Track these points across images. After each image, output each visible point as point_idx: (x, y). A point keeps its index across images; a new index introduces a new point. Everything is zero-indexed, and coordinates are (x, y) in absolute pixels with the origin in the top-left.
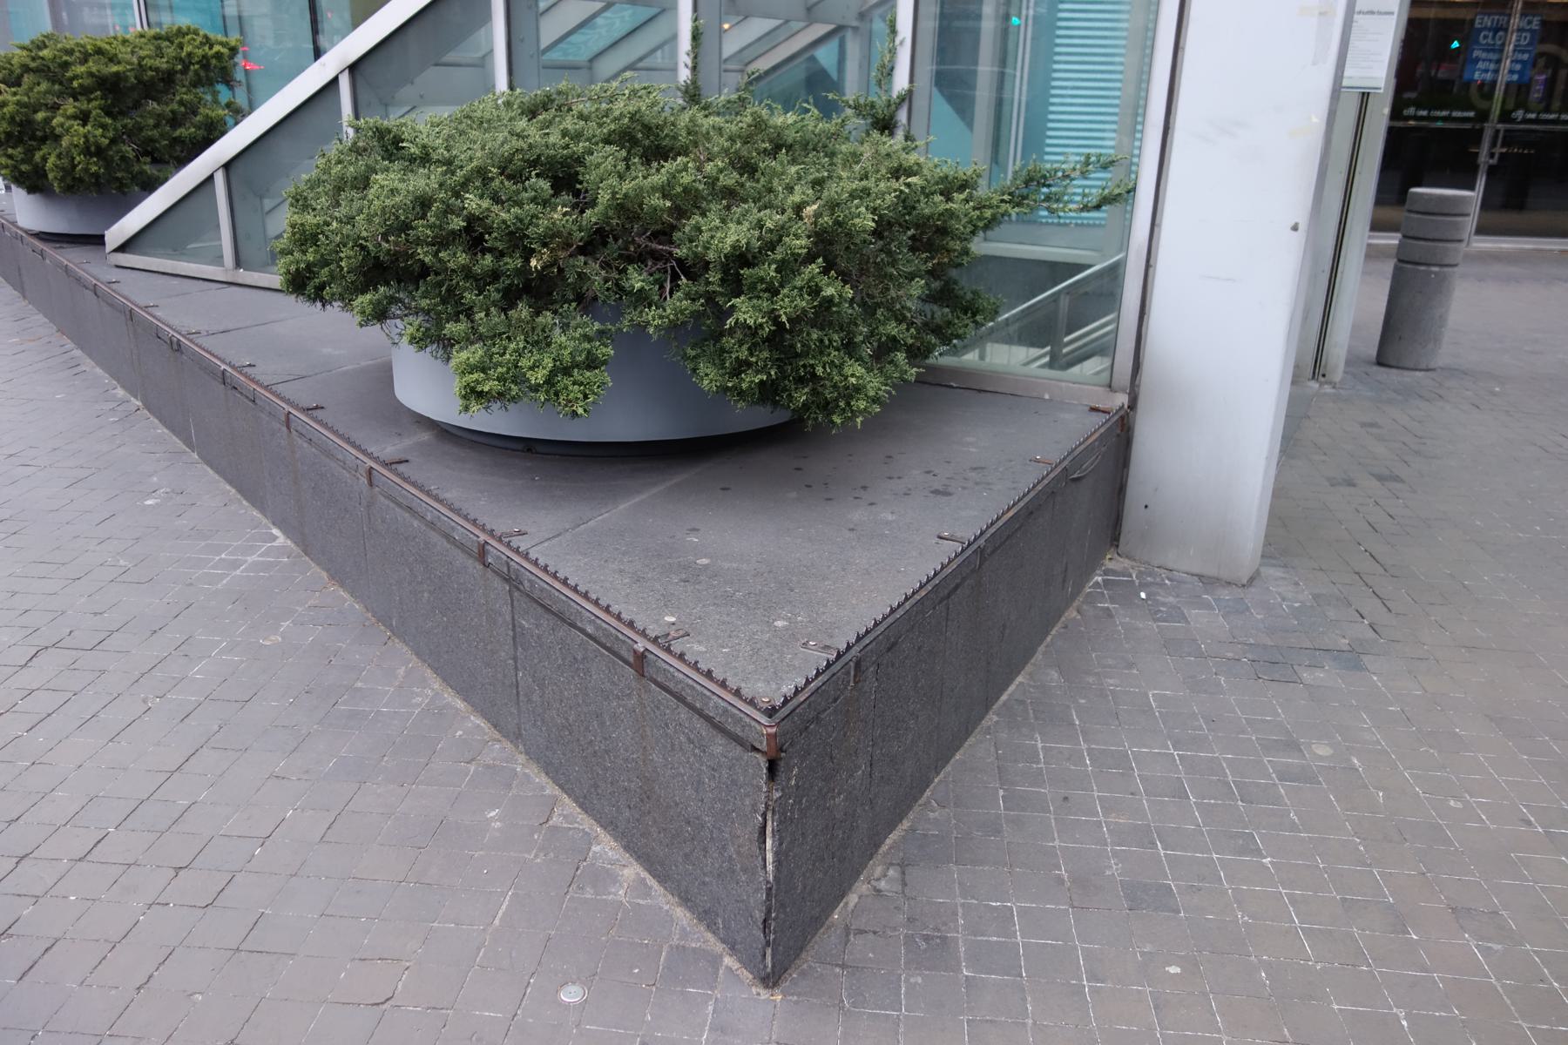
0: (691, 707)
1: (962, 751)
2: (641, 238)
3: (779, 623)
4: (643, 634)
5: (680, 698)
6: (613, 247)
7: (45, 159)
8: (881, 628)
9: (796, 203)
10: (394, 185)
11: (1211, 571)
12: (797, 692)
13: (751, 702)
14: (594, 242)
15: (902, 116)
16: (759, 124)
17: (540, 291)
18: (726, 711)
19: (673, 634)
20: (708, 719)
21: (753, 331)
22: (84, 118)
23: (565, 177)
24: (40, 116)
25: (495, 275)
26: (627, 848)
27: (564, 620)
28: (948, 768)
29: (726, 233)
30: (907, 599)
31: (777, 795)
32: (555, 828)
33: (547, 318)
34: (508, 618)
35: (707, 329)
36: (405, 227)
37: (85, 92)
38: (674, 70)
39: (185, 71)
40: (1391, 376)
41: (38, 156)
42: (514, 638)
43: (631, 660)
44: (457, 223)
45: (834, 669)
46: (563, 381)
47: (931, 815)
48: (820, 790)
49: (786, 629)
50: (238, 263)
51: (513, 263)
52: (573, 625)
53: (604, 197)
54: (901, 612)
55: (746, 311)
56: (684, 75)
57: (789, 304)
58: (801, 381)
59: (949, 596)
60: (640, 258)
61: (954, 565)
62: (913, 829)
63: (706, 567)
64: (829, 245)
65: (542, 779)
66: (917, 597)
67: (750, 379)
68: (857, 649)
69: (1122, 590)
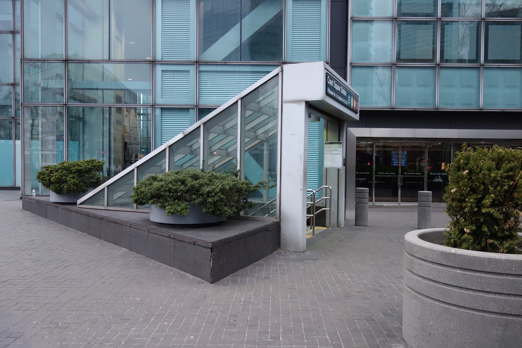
2: (195, 191)
6: (190, 192)
7: (64, 186)
9: (218, 185)
10: (156, 184)
11: (296, 250)
14: (187, 192)
15: (239, 174)
16: (213, 175)
17: (179, 198)
21: (211, 203)
22: (73, 178)
23: (183, 182)
24: (64, 177)
25: (172, 196)
29: (207, 189)
33: (180, 202)
35: (204, 203)
36: (159, 189)
37: (74, 173)
38: (199, 166)
39: (94, 168)
40: (357, 227)
41: (62, 186)
44: (167, 189)
46: (182, 211)
50: (108, 206)
51: (175, 194)
53: (189, 185)
55: (210, 200)
56: (201, 167)
57: (216, 198)
58: (218, 210)
60: (194, 194)
64: (222, 191)
67: (211, 210)
69: (280, 254)
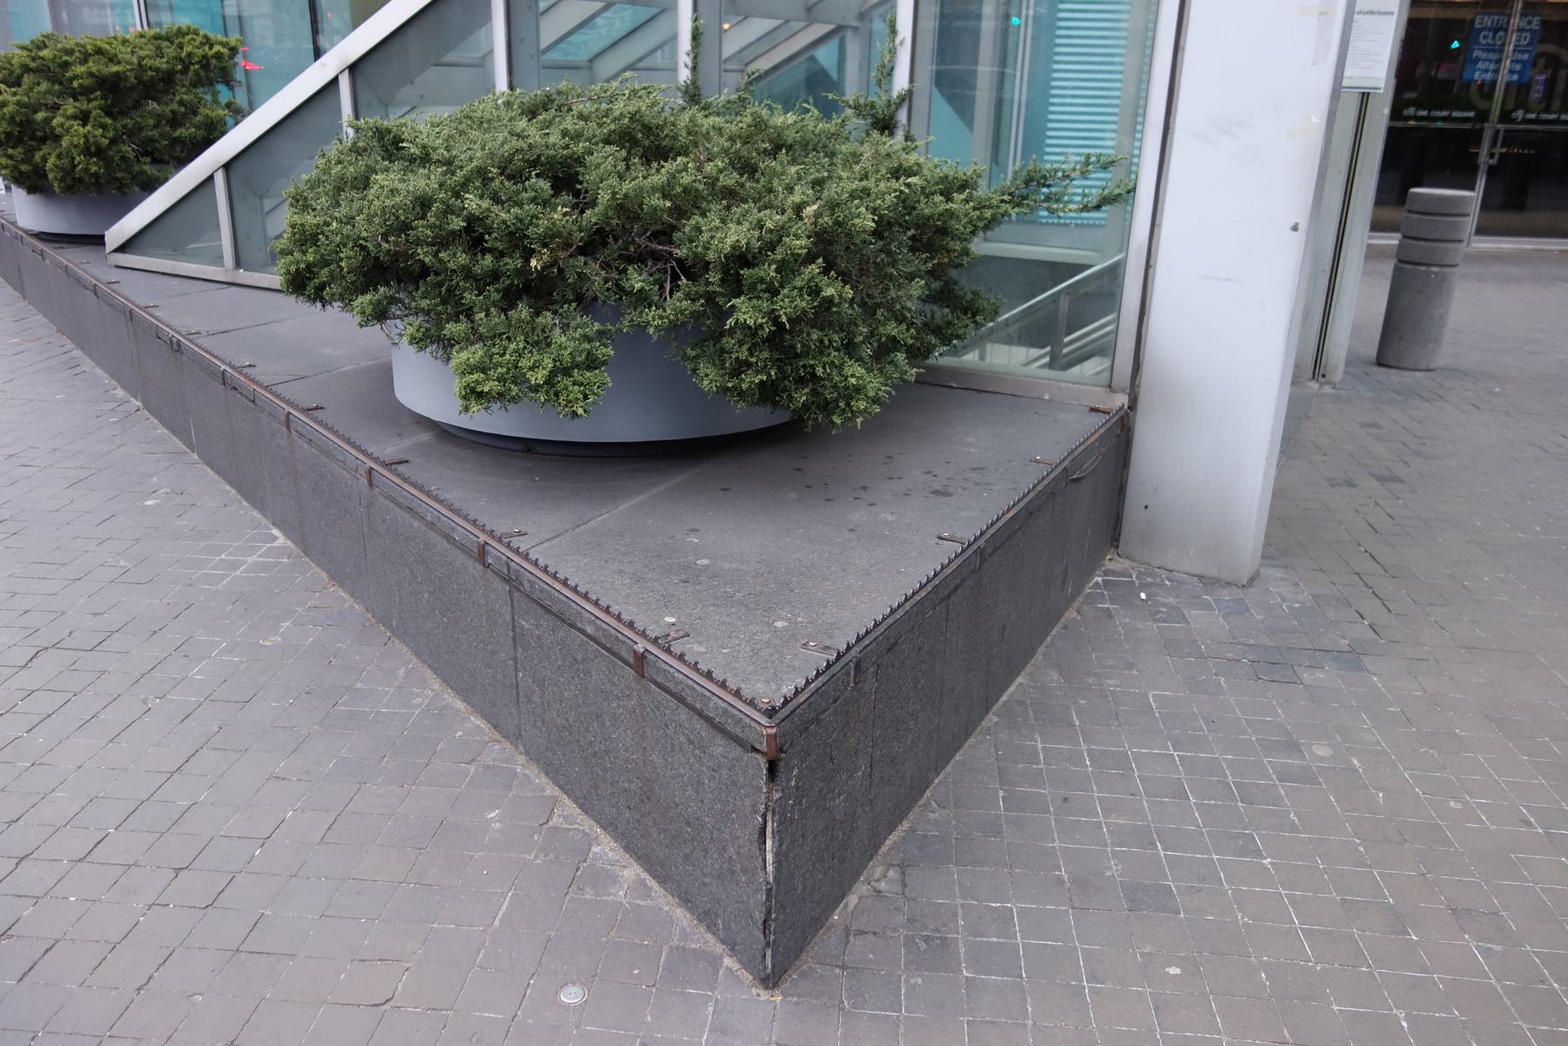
0: (691, 708)
1: (962, 752)
2: (641, 239)
3: (779, 624)
4: (643, 634)
5: (680, 699)
6: (613, 247)
7: (45, 159)
8: (881, 629)
9: (796, 203)
10: (394, 185)
11: (1211, 571)
12: (797, 693)
13: (751, 703)
14: (594, 243)
15: (902, 116)
16: (759, 125)
17: (540, 291)
18: (726, 711)
19: (673, 634)
20: (708, 720)
21: (753, 331)
22: (84, 118)
23: (565, 177)
24: (40, 116)
25: (495, 276)
26: (627, 849)
27: (564, 621)
28: (948, 769)
29: (726, 233)
30: (907, 600)
31: (777, 796)
32: (555, 829)
33: (547, 318)
34: (508, 619)
35: (707, 329)
36: (405, 227)
37: (85, 92)
38: (674, 70)
39: (185, 71)
40: (1391, 377)
41: (38, 156)
42: (514, 639)
43: (631, 660)
44: (457, 223)
45: (834, 669)
46: (563, 381)
47: (931, 816)
48: (820, 791)
49: (786, 629)
50: (238, 264)
51: (513, 263)
52: (573, 626)
53: (604, 197)
54: (901, 612)
55: (746, 311)
56: (684, 75)
57: (789, 304)
58: (801, 381)
59: (949, 596)
60: (640, 259)
61: (954, 566)
62: (913, 830)
63: (706, 567)
64: (829, 245)
65: (542, 780)
66: (917, 598)
67: (750, 379)
68: (857, 649)
69: (1122, 591)
